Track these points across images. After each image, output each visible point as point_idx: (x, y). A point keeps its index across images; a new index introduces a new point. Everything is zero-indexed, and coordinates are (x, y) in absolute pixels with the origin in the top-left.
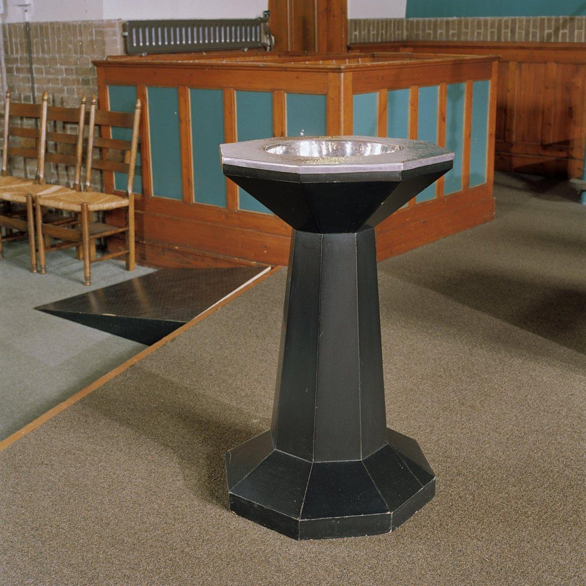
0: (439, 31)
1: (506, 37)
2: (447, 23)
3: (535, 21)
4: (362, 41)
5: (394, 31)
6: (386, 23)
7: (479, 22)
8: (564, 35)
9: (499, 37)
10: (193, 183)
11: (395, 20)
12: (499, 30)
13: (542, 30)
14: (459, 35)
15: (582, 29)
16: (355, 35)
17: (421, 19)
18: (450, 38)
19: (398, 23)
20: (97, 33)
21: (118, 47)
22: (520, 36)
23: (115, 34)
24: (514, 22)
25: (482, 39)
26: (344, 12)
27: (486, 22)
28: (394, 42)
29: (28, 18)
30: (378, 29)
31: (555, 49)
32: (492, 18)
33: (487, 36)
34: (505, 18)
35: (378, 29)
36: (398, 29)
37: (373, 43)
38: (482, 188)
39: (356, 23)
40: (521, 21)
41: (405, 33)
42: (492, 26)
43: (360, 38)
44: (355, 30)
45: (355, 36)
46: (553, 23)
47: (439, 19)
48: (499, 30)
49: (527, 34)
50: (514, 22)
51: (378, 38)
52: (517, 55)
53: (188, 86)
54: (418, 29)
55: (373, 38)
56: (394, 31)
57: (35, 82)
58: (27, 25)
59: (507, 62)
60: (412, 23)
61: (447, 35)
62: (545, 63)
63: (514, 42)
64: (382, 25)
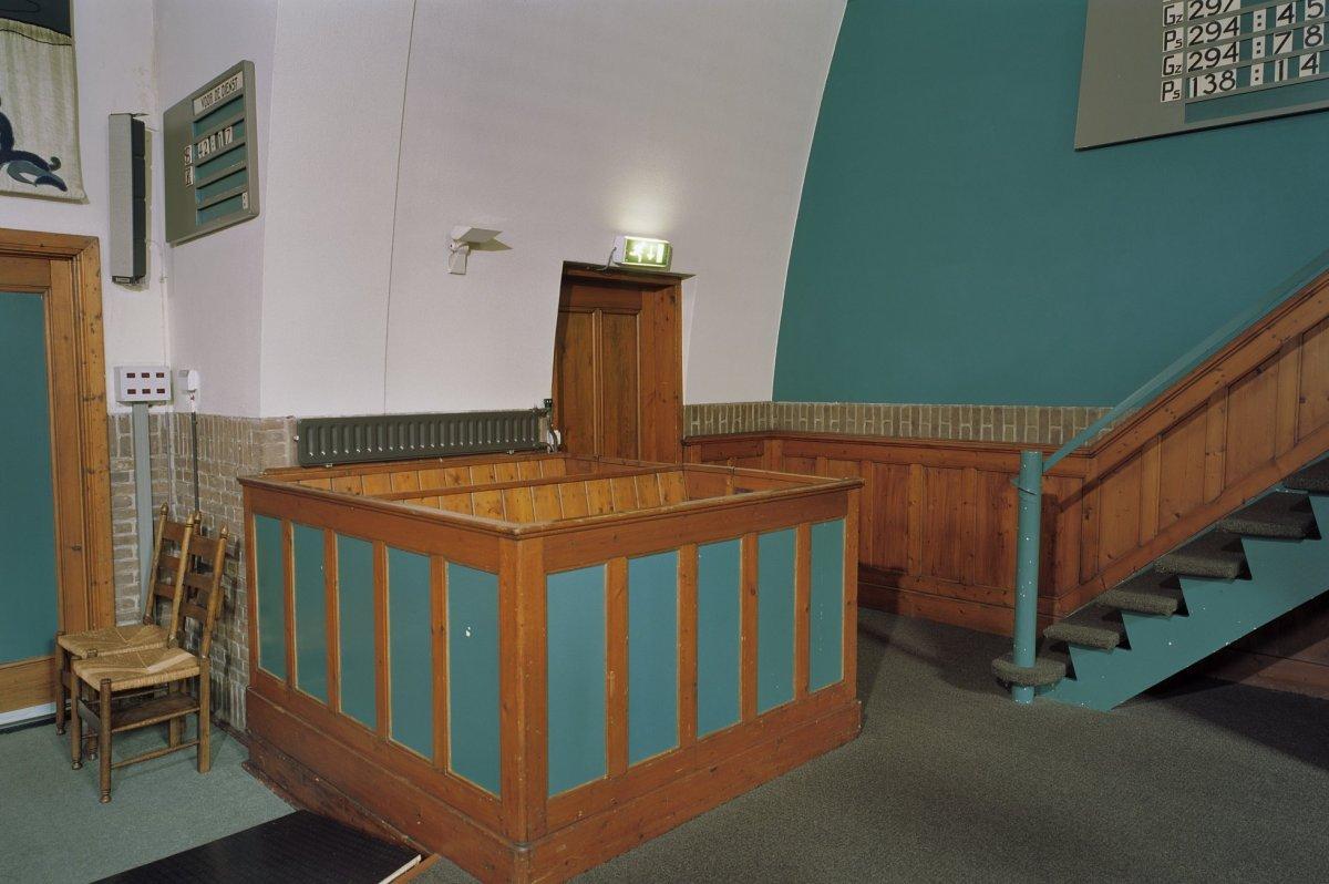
0: (816, 420)
1: (905, 430)
2: (827, 409)
3: (945, 411)
4: (705, 433)
5: (756, 419)
6: (745, 409)
7: (869, 410)
8: (987, 431)
9: (896, 430)
10: (340, 680)
11: (757, 404)
12: (896, 421)
13: (956, 423)
14: (843, 425)
15: (1012, 423)
16: (693, 427)
17: (792, 403)
18: (831, 430)
19: (762, 408)
20: (257, 435)
21: (286, 456)
22: (925, 431)
23: (281, 438)
24: (915, 410)
25: (873, 432)
26: (678, 397)
27: (878, 409)
28: (757, 432)
29: (194, 407)
30: (731, 417)
31: (975, 450)
32: (887, 405)
33: (879, 429)
34: (905, 405)
35: (731, 417)
36: (762, 416)
37: (723, 434)
38: (837, 688)
39: (696, 410)
40: (925, 411)
41: (772, 421)
42: (887, 416)
43: (702, 430)
44: (695, 419)
45: (695, 427)
46: (971, 414)
47: (816, 404)
48: (896, 421)
49: (935, 428)
50: (915, 410)
51: (730, 428)
52: (921, 456)
53: (335, 531)
54: (788, 416)
55: (724, 429)
56: (756, 419)
57: (200, 494)
58: (194, 415)
59: (909, 465)
60: (781, 408)
61: (827, 426)
62: (962, 468)
63: (917, 438)
64: (737, 412)
